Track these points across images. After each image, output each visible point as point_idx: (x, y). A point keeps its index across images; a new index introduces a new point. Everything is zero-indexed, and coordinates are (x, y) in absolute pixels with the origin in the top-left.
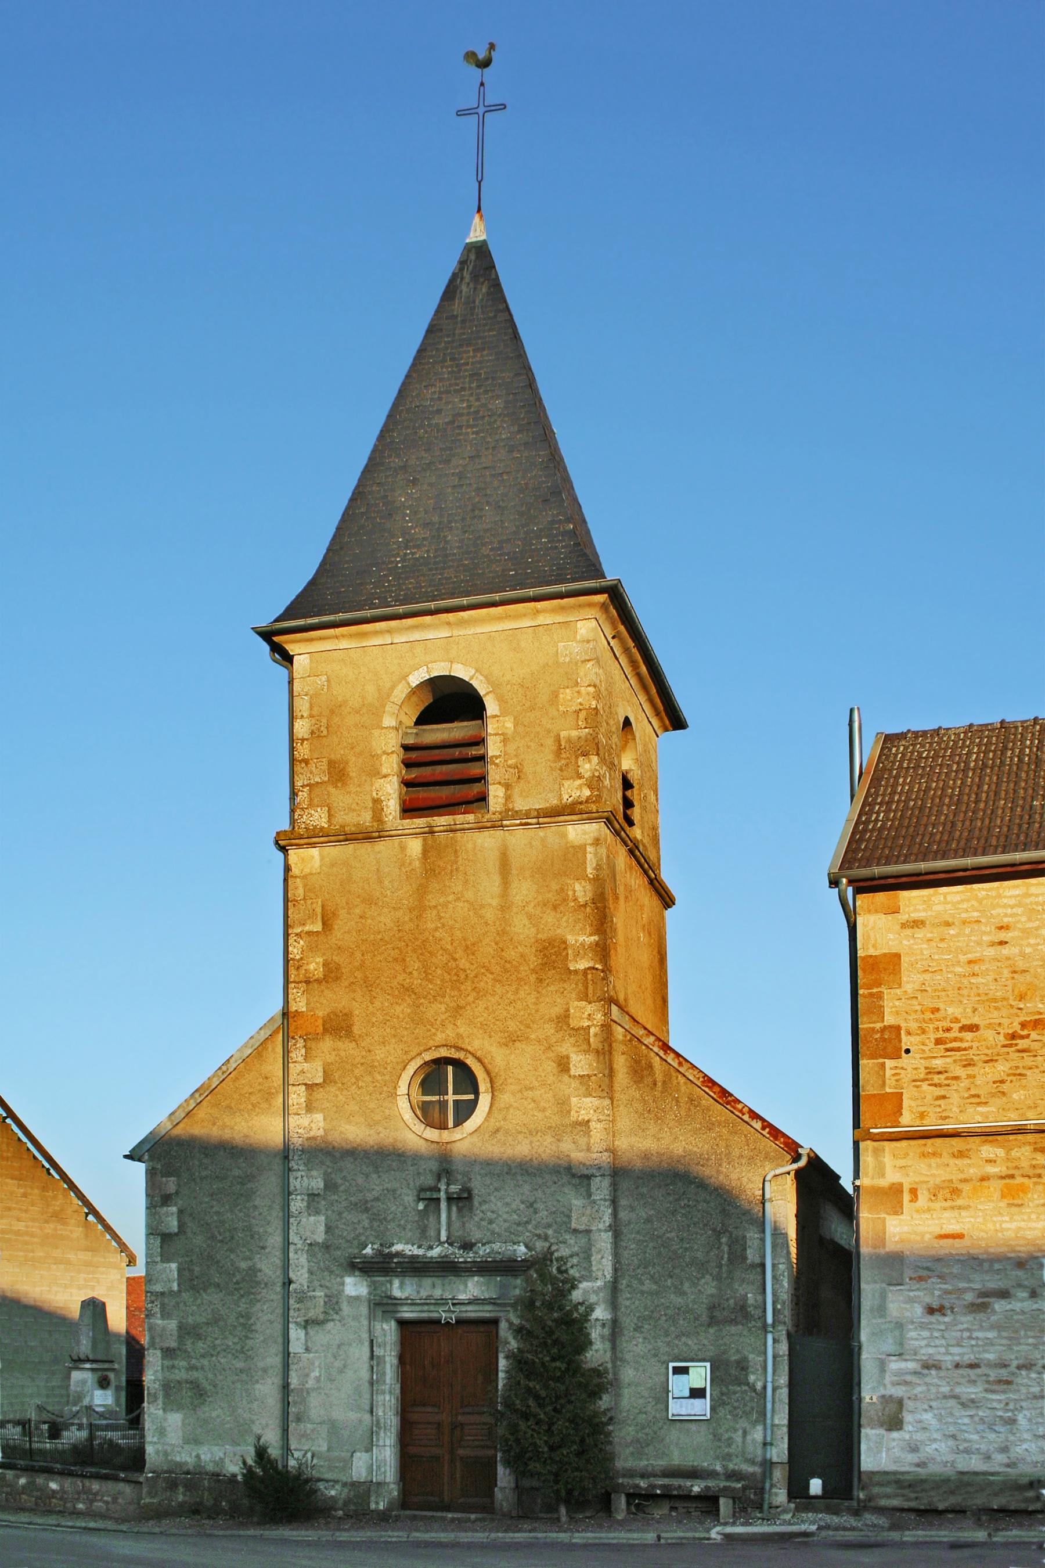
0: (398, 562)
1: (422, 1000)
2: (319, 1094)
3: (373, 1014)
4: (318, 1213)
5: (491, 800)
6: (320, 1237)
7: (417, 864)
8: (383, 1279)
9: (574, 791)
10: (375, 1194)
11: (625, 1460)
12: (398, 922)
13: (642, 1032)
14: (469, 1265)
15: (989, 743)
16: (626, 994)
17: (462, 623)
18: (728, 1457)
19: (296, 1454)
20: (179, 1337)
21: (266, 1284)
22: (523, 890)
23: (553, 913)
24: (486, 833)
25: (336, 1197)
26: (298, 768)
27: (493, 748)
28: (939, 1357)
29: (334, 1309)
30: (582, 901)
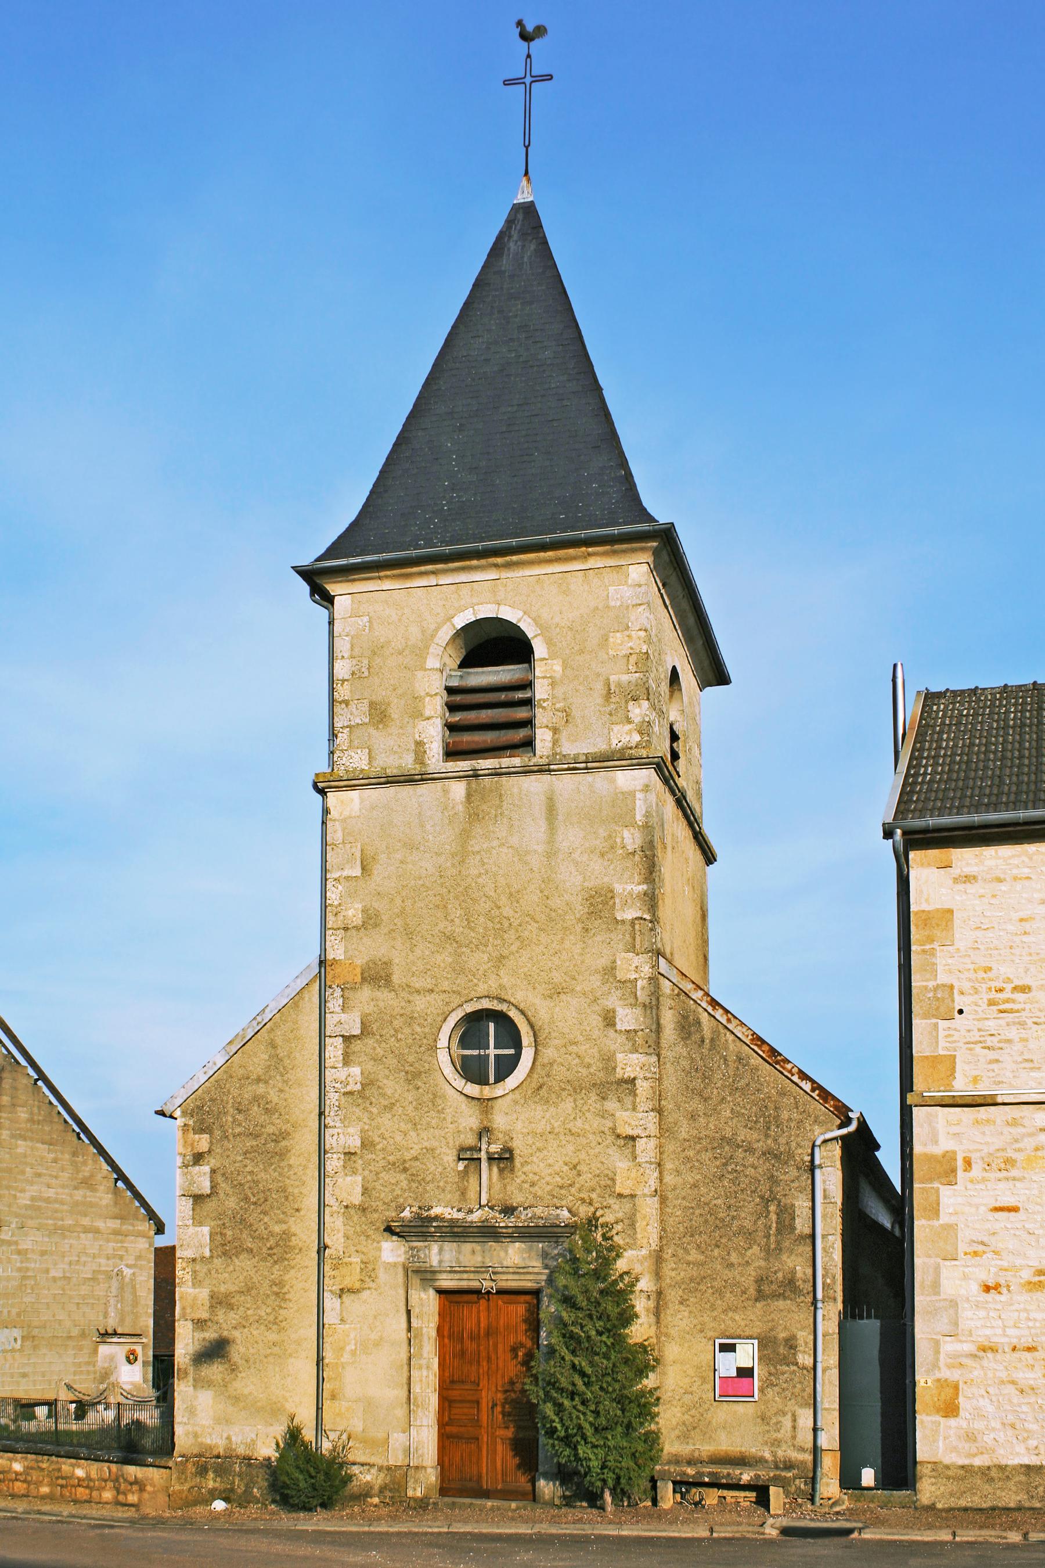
0: (445, 505)
1: (464, 949)
2: (357, 1046)
3: (413, 963)
4: (354, 1172)
5: (538, 744)
6: (357, 1199)
7: (460, 808)
8: (421, 1244)
9: (623, 736)
10: (413, 1153)
11: (671, 1446)
12: (440, 870)
13: (691, 986)
14: (510, 1230)
15: (1024, 703)
16: (672, 948)
17: (508, 566)
18: (777, 1443)
19: (333, 1436)
20: (211, 1307)
21: (300, 1250)
22: (570, 837)
23: (600, 861)
24: (533, 778)
25: (374, 1156)
26: (337, 709)
27: (541, 691)
28: (995, 1339)
29: (370, 1277)
30: (630, 848)
